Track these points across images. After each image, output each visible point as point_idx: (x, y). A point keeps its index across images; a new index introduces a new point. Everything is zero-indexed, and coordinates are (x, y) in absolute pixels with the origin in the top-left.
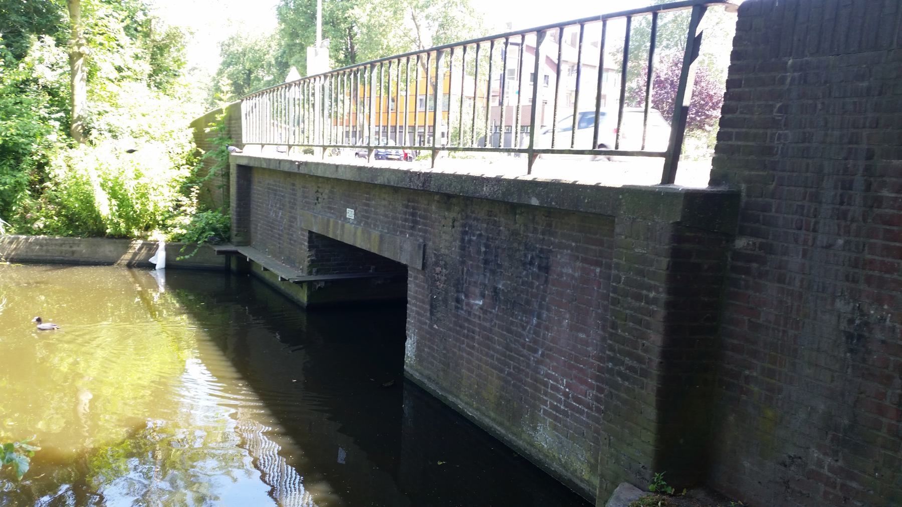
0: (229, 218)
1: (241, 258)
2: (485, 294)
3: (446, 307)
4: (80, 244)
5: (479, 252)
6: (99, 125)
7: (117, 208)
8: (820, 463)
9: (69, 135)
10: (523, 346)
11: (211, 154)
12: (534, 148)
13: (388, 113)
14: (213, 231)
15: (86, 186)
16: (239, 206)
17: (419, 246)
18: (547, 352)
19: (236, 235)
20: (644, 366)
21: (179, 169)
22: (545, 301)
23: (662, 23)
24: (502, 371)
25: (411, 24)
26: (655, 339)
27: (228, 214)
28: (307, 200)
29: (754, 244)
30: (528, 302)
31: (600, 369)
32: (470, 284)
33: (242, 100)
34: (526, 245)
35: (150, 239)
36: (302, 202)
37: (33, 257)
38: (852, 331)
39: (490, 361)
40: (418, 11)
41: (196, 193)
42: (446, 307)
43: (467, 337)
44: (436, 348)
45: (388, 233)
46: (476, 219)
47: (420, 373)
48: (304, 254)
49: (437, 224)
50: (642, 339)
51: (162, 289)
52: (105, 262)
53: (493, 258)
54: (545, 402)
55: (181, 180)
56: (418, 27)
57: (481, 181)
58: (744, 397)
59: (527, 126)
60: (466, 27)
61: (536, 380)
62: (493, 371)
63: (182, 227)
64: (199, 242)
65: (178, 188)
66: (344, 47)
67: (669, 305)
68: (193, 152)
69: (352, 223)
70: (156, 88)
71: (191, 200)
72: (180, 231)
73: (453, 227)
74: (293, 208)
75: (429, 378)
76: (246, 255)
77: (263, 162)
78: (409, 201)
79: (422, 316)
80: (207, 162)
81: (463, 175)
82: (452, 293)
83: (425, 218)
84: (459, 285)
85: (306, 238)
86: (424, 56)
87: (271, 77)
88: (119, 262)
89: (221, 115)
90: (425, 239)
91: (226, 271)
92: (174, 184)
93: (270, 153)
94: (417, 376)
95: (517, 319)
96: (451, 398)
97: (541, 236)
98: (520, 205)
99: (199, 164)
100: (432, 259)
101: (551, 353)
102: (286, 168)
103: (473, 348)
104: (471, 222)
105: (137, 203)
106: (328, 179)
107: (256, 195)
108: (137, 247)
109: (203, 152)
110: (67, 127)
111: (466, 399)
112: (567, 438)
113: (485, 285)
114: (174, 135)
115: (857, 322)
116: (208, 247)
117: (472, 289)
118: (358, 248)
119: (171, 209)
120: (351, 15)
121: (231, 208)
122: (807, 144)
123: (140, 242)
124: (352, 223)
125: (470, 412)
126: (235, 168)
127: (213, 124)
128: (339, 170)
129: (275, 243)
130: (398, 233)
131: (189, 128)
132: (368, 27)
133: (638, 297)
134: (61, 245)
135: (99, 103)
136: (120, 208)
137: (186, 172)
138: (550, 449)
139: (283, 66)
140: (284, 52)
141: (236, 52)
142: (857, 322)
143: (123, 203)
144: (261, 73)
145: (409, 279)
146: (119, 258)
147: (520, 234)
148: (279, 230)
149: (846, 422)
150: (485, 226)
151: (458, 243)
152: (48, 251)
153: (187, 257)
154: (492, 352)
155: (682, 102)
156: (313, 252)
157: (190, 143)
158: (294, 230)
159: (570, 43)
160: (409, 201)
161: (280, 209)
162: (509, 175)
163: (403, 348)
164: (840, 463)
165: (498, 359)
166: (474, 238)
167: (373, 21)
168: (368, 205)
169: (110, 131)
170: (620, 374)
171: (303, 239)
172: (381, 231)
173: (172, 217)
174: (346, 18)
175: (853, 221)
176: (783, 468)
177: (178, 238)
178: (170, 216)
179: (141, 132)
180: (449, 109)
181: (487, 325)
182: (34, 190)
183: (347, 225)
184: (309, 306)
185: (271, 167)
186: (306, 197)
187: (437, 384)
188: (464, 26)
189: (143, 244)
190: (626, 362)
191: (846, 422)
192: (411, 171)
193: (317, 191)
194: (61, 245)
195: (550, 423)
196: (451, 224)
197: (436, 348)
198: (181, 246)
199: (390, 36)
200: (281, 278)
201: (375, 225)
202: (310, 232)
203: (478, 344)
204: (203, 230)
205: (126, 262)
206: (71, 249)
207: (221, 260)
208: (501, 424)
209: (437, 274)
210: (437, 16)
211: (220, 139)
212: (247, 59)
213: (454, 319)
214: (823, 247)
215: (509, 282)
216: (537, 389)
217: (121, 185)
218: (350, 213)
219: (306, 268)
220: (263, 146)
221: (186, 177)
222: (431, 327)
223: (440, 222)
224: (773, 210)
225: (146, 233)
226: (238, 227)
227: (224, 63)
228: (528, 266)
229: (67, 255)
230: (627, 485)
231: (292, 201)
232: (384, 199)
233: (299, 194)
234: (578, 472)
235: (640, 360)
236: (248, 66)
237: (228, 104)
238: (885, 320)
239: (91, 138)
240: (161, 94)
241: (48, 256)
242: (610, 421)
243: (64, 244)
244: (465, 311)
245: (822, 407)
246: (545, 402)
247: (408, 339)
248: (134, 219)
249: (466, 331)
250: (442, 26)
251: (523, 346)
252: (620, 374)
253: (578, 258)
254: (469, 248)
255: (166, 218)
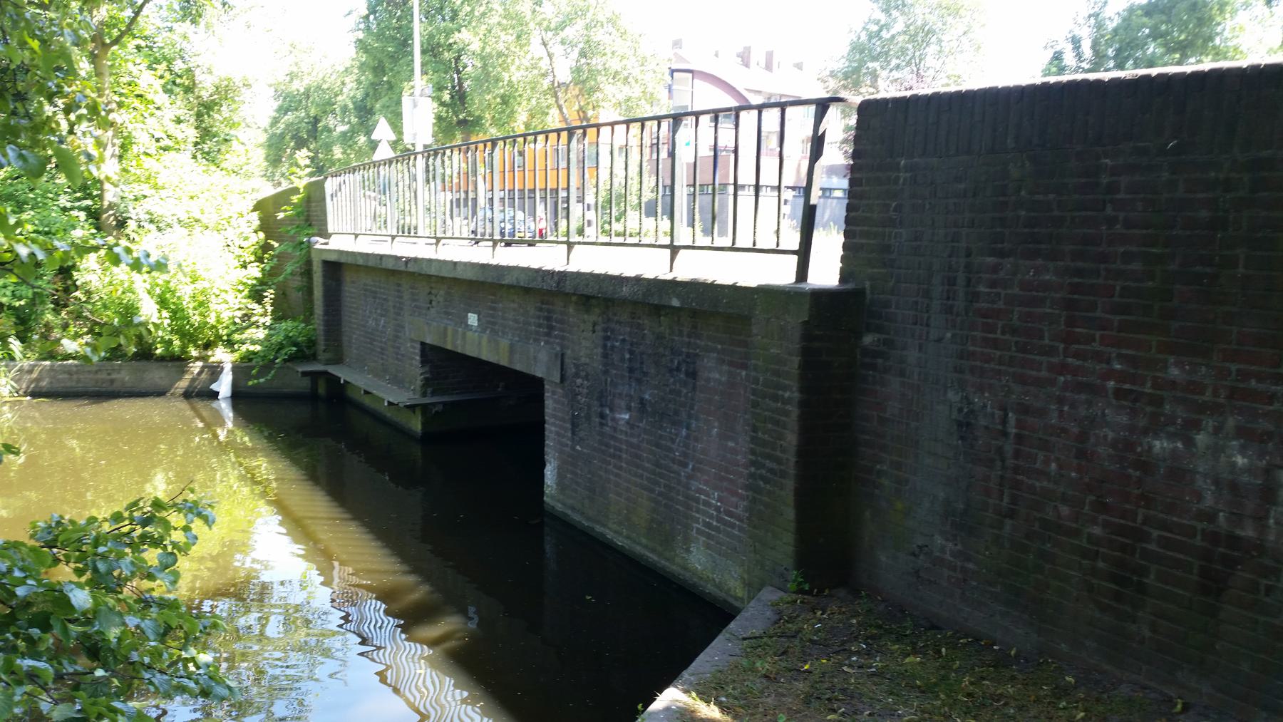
0: (314, 329)
1: (332, 380)
2: (631, 407)
3: (589, 424)
4: (120, 370)
5: (623, 360)
6: (137, 214)
7: (169, 321)
8: (943, 550)
9: (98, 228)
10: (673, 461)
11: (287, 247)
12: (675, 244)
13: (514, 171)
14: (294, 346)
15: (128, 294)
16: (326, 313)
17: (556, 355)
18: (697, 465)
19: (324, 351)
20: (782, 467)
21: (246, 267)
22: (693, 409)
23: (888, 36)
24: (652, 491)
25: (541, 52)
26: (791, 439)
27: (312, 324)
28: (418, 304)
29: (879, 340)
30: (676, 413)
31: (752, 476)
32: (614, 396)
33: (326, 178)
34: (672, 349)
35: (212, 359)
36: (411, 305)
37: (60, 390)
38: (961, 419)
39: (638, 480)
40: (550, 34)
41: (271, 299)
42: (589, 424)
43: (614, 456)
44: (579, 472)
45: (519, 341)
46: (619, 322)
47: (564, 504)
48: (415, 370)
49: (576, 329)
50: (780, 440)
51: (230, 425)
52: (154, 393)
53: (638, 366)
54: (697, 521)
55: (250, 282)
56: (550, 56)
57: (620, 280)
58: (877, 491)
59: (708, 185)
60: (616, 54)
61: (687, 497)
62: (643, 491)
63: (254, 342)
64: (277, 361)
65: (246, 292)
66: (449, 85)
67: (803, 404)
68: (261, 244)
69: (476, 331)
70: (204, 160)
71: (264, 307)
72: (252, 348)
73: (594, 332)
74: (399, 314)
75: (573, 509)
76: (340, 375)
77: (359, 258)
78: (542, 303)
79: (564, 436)
80: (281, 257)
81: (601, 274)
82: (596, 408)
83: (561, 322)
84: (603, 398)
85: (418, 351)
86: (553, 136)
87: (345, 128)
88: (172, 391)
89: (298, 196)
90: (563, 347)
91: (311, 398)
92: (241, 287)
93: (365, 246)
94: (559, 507)
95: (665, 431)
96: (598, 528)
97: (687, 340)
98: (664, 307)
99: (271, 260)
100: (571, 370)
101: (702, 466)
102: (390, 265)
103: (620, 468)
104: (613, 325)
105: (194, 315)
106: (443, 278)
107: (348, 299)
108: (197, 370)
109: (276, 245)
110: (94, 215)
111: (615, 527)
112: (720, 555)
113: (631, 397)
114: (233, 222)
115: (965, 410)
116: (288, 368)
117: (617, 401)
118: (484, 361)
119: (237, 320)
120: (458, 41)
121: (316, 316)
122: (919, 243)
123: (200, 364)
124: (476, 331)
125: (620, 541)
126: (320, 265)
127: (288, 208)
128: (458, 267)
129: (376, 359)
130: (531, 341)
131: (252, 211)
132: (482, 58)
133: (775, 398)
134: (96, 372)
135: (135, 185)
136: (172, 321)
137: (255, 272)
138: (704, 570)
139: (364, 112)
140: (367, 95)
141: (296, 93)
142: (965, 410)
143: (177, 313)
144: (331, 121)
145: (546, 394)
146: (171, 386)
147: (665, 338)
148: (381, 342)
149: (962, 506)
150: (628, 329)
151: (600, 350)
152: (78, 381)
153: (262, 380)
154: (641, 472)
155: (809, 201)
156: (427, 369)
157: (256, 232)
158: (401, 341)
159: (764, 66)
160: (542, 303)
161: (382, 315)
162: (649, 274)
163: (542, 476)
164: (959, 547)
165: (648, 479)
166: (617, 344)
167: (488, 50)
168: (494, 309)
169: (151, 221)
170: (762, 478)
171: (414, 353)
172: (511, 340)
173: (242, 330)
174: (450, 45)
175: (958, 315)
176: (912, 558)
177: (249, 357)
178: (237, 330)
179: (191, 220)
180: (597, 163)
181: (635, 440)
182: (56, 303)
183: (469, 334)
184: (425, 433)
185: (370, 264)
186: (415, 300)
187: (583, 513)
188: (613, 53)
189: (203, 368)
190: (767, 465)
191: (962, 506)
192: (544, 269)
193: (430, 293)
194: (96, 372)
195: (704, 541)
196: (591, 328)
197: (579, 472)
198: (253, 368)
199: (513, 68)
200: (388, 402)
201: (504, 333)
202: (423, 344)
203: (627, 463)
204: (281, 347)
205: (181, 391)
206: (109, 377)
207: (305, 384)
208: (653, 550)
209: (578, 387)
210: (575, 40)
211: (297, 227)
212: (312, 103)
213: (598, 438)
214: (935, 341)
215: (656, 392)
216: (689, 508)
217: (173, 292)
218: (473, 319)
219: (418, 388)
220: (356, 237)
221: (256, 278)
222: (573, 448)
223: (579, 327)
224: (893, 307)
225: (206, 352)
226: (326, 340)
227: (279, 109)
228: (675, 373)
229: (104, 385)
230: (770, 588)
231: (398, 305)
232: (513, 301)
233: (406, 296)
234: (732, 590)
235: (778, 461)
236: (313, 112)
237: (306, 181)
238: (986, 407)
239: (128, 231)
240: (213, 168)
241: (80, 387)
242: (755, 527)
243: (100, 370)
244: (611, 427)
245: (942, 495)
246: (697, 521)
247: (548, 465)
248: (191, 335)
249: (612, 450)
250: (583, 54)
251: (673, 461)
252: (762, 478)
253: (724, 361)
254: (612, 355)
255: (234, 332)
